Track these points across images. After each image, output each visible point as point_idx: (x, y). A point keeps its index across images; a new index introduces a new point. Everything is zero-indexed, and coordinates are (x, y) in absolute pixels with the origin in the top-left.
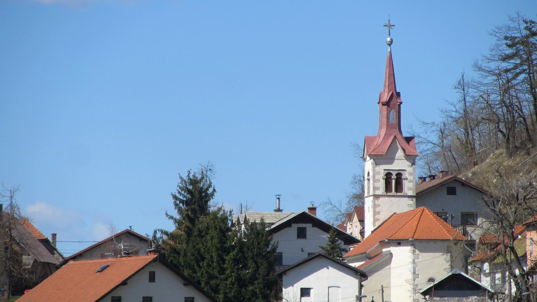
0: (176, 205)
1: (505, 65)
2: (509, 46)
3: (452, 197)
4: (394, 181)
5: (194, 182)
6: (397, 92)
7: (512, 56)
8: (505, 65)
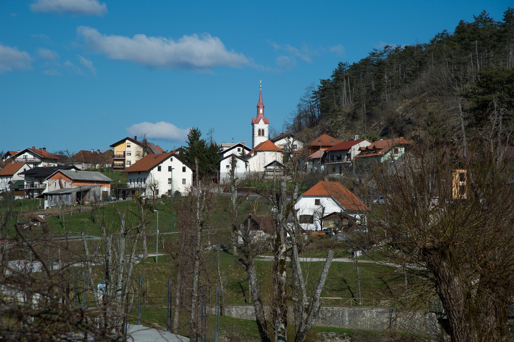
0: (189, 138)
1: (311, 100)
2: (313, 94)
3: (314, 203)
4: (261, 132)
5: (194, 131)
6: (258, 153)
7: (430, 44)
8: (311, 100)
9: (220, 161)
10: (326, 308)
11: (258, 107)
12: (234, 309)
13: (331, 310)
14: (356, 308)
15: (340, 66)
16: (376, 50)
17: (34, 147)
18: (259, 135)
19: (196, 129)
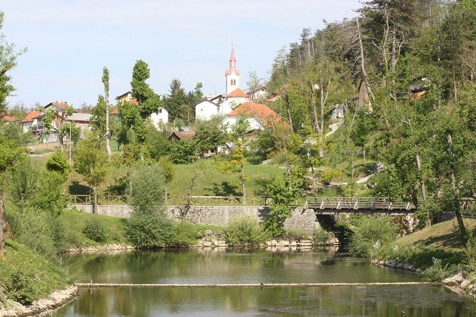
9: (195, 105)
10: (206, 207)
11: (230, 61)
12: (109, 208)
13: (210, 209)
14: (236, 207)
15: (304, 31)
16: (336, 21)
17: (57, 102)
18: (232, 84)
19: (177, 80)
